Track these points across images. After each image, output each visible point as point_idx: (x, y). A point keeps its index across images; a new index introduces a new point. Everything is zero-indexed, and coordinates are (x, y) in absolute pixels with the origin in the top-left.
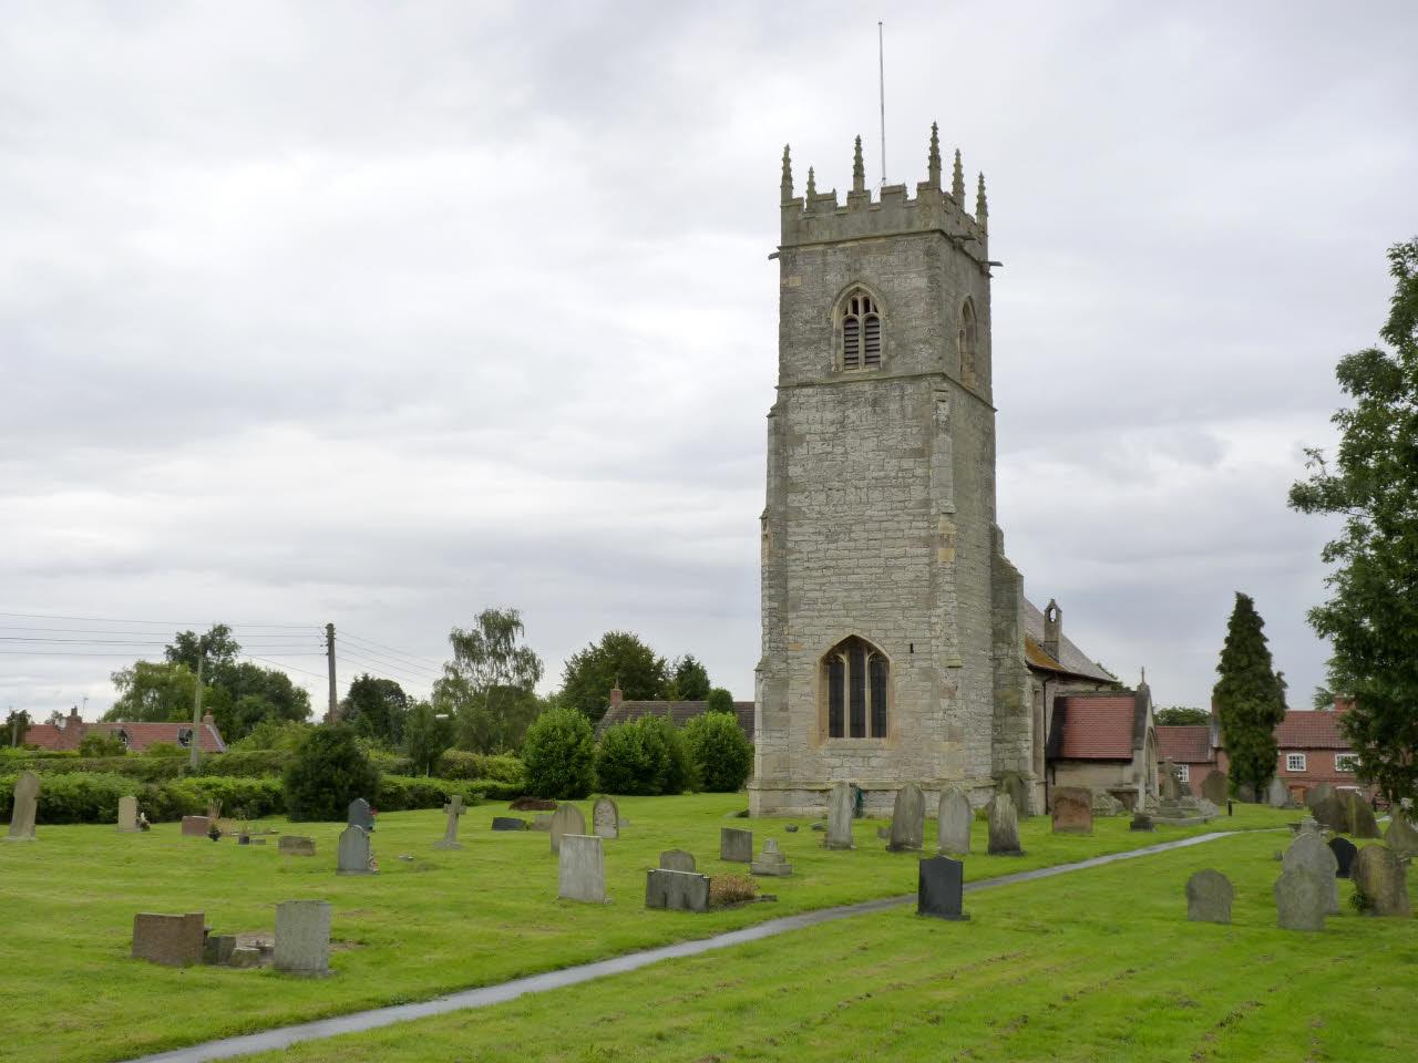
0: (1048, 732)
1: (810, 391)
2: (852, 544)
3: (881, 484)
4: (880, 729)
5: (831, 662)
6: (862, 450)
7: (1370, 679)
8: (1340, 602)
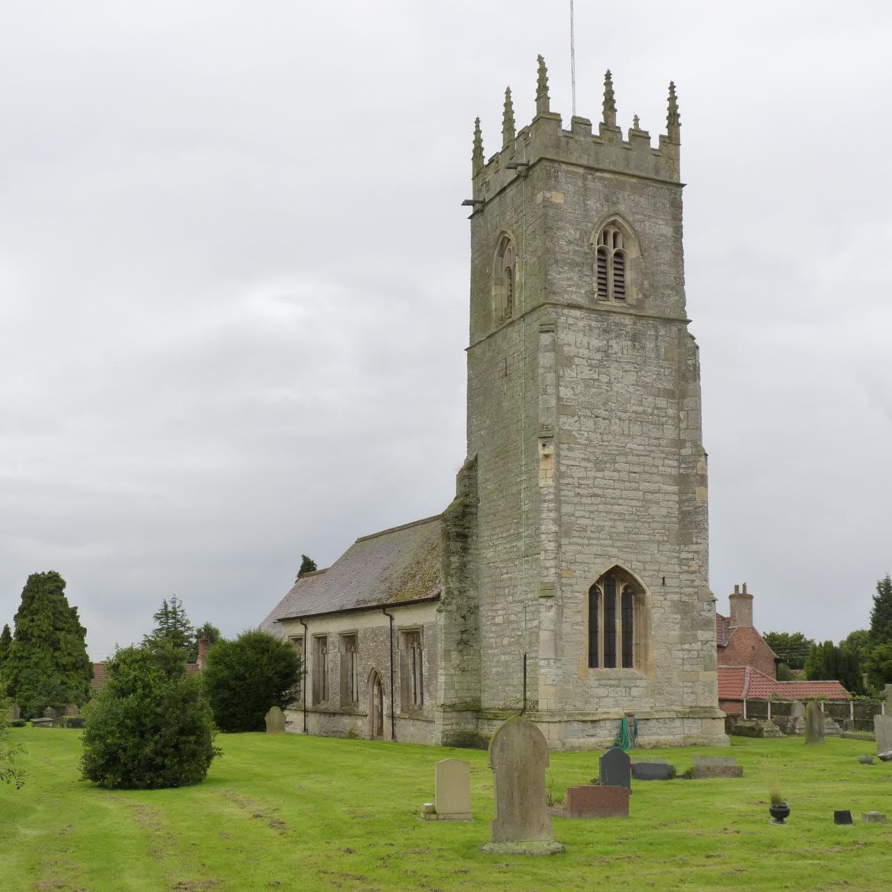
3: (639, 418)
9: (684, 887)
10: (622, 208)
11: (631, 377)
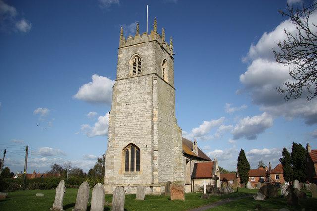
0: (192, 172)
1: (122, 80)
2: (132, 119)
3: (139, 102)
4: (138, 169)
5: (125, 149)
6: (135, 94)
7: (54, 119)
8: (119, 208)
9: (194, 209)
10: (138, 52)
11: (137, 92)
